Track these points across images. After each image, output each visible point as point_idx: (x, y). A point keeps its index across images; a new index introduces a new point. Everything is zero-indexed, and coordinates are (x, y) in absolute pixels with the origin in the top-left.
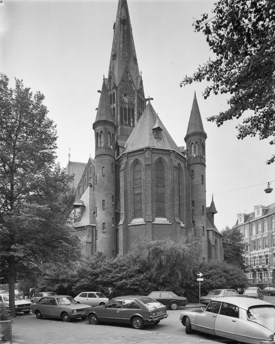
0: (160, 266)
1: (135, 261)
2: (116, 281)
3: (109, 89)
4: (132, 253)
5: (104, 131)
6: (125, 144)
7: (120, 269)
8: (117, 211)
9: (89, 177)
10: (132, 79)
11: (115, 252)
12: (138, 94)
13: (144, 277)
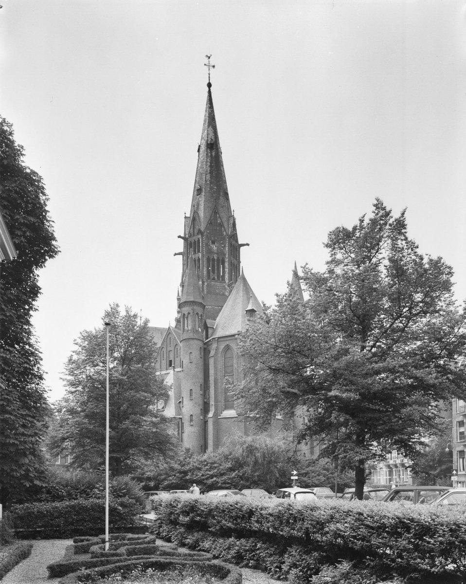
0: (256, 462)
1: (226, 458)
2: (207, 479)
3: (192, 234)
4: (224, 450)
5: (191, 312)
6: (215, 323)
7: (211, 467)
8: (205, 400)
9: (168, 350)
10: (222, 221)
11: (204, 448)
12: (229, 240)
13: (236, 475)
